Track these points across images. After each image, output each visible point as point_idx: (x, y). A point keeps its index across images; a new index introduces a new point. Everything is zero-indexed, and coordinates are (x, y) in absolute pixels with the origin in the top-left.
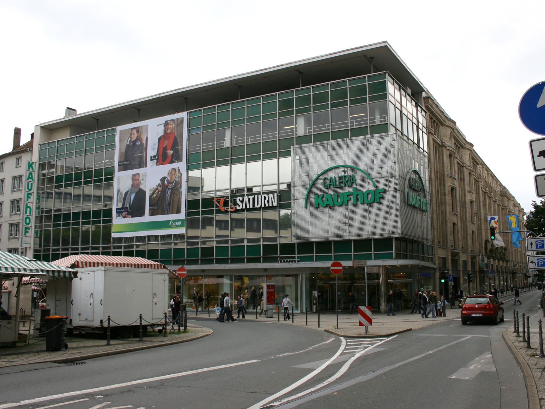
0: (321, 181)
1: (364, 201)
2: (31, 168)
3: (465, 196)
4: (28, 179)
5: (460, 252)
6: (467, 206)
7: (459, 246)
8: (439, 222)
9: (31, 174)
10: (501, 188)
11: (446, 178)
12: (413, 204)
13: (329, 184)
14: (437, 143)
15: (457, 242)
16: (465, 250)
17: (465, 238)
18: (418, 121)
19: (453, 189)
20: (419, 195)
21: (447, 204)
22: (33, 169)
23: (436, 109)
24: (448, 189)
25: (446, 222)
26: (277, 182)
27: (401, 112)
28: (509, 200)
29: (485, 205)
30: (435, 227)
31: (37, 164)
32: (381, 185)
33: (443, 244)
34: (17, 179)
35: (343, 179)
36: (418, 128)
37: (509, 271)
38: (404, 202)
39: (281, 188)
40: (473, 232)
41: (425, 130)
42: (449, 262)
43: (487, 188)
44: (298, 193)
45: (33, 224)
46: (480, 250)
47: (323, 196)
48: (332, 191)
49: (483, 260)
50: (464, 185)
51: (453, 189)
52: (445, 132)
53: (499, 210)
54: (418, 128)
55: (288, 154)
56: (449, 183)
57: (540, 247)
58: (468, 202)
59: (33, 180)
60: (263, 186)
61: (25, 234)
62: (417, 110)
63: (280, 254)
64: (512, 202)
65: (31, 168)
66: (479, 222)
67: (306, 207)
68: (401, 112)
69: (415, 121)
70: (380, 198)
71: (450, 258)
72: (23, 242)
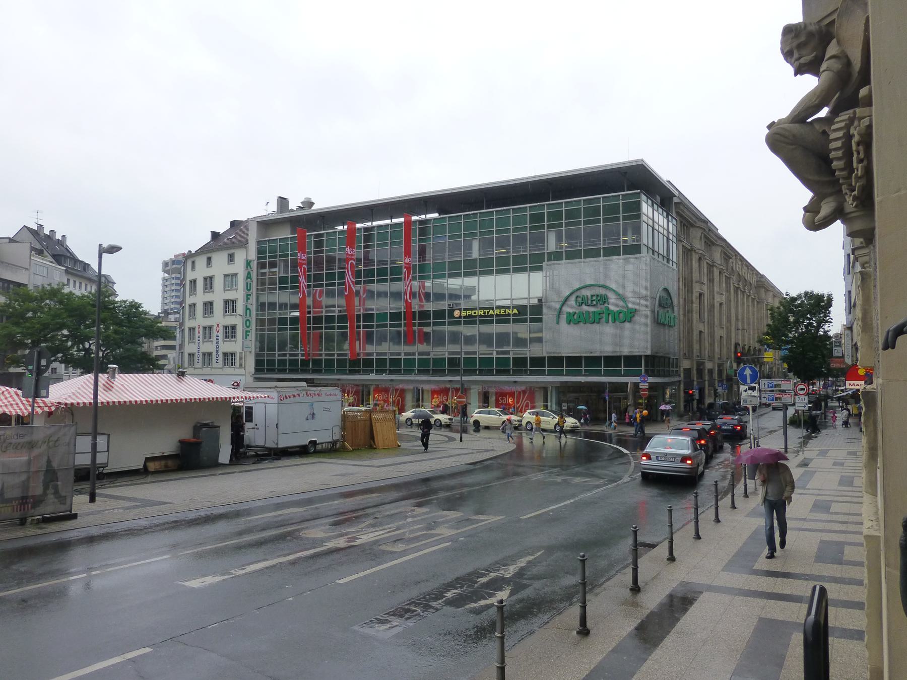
0: (573, 297)
1: (615, 320)
2: (249, 267)
3: (713, 298)
4: (247, 279)
5: (706, 361)
6: (715, 310)
7: (705, 355)
8: (685, 331)
9: (249, 273)
10: (757, 277)
11: (694, 284)
12: (662, 322)
13: (581, 302)
14: (686, 248)
15: (703, 352)
16: (711, 359)
17: (712, 345)
18: (668, 232)
19: (701, 295)
20: (668, 311)
21: (694, 312)
22: (251, 268)
23: (688, 213)
24: (695, 295)
25: (692, 331)
26: (527, 296)
27: (653, 228)
28: (768, 290)
29: (737, 302)
30: (681, 338)
31: (255, 262)
32: (633, 305)
33: (688, 356)
34: (230, 278)
35: (594, 298)
36: (668, 239)
37: (763, 375)
38: (654, 322)
39: (531, 302)
40: (721, 337)
41: (675, 240)
42: (695, 372)
43: (740, 281)
44: (549, 310)
45: (253, 326)
46: (728, 355)
47: (575, 313)
48: (584, 309)
49: (731, 367)
50: (713, 286)
51: (701, 295)
52: (696, 234)
53: (754, 305)
54: (668, 239)
55: (539, 269)
56: (697, 289)
57: (771, 387)
58: (717, 305)
59: (251, 280)
60: (513, 299)
61: (246, 338)
62: (668, 221)
63: (530, 367)
64: (771, 294)
65: (249, 267)
66: (729, 325)
67: (558, 323)
68: (653, 228)
69: (665, 233)
70: (631, 317)
71: (695, 368)
72: (245, 346)
